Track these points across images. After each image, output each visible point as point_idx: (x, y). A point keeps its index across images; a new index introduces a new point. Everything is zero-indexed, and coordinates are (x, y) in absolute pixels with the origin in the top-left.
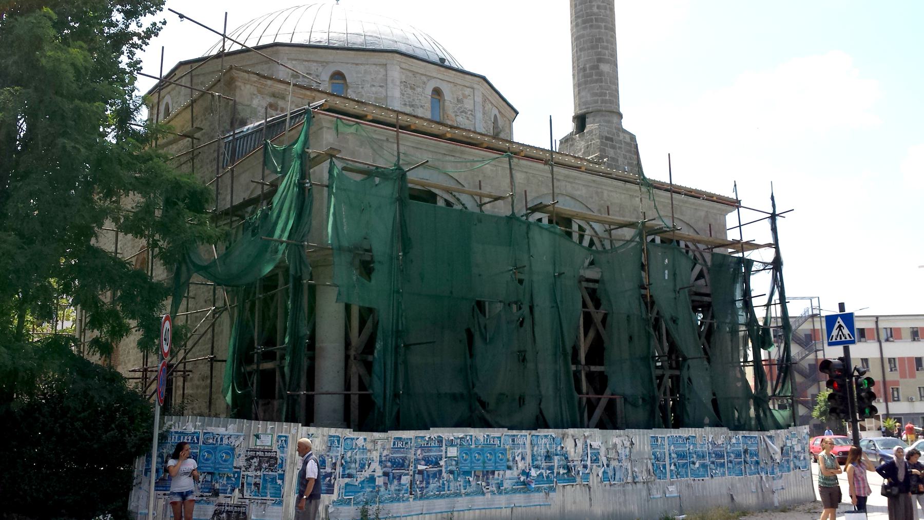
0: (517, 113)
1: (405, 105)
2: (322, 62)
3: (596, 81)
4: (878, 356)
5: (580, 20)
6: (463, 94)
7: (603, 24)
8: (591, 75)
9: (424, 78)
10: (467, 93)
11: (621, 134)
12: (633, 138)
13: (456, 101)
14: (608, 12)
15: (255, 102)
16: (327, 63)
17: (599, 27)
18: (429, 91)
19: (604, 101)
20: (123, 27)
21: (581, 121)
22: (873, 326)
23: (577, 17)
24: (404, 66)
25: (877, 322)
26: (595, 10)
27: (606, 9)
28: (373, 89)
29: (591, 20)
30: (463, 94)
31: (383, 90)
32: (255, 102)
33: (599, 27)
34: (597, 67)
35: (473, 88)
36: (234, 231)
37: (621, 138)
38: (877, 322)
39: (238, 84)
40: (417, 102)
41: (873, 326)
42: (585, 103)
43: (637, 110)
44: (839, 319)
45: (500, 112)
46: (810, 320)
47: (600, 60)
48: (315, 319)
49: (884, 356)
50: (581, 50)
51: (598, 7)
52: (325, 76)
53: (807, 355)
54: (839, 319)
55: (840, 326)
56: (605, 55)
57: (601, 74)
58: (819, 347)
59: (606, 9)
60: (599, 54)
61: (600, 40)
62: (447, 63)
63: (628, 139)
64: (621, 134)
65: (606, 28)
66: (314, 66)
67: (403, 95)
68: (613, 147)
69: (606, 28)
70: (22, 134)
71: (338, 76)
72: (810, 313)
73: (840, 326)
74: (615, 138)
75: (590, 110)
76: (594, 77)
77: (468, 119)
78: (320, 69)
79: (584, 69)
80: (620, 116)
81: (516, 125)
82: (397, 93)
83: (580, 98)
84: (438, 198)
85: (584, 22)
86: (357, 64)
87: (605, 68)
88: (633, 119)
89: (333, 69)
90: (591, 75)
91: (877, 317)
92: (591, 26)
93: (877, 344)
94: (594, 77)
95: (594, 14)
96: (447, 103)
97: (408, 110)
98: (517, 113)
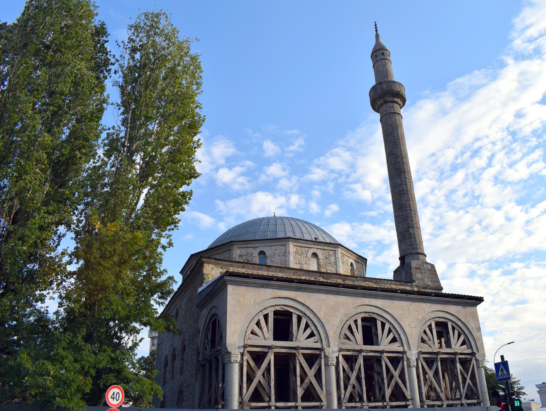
5: (397, 208)
8: (405, 235)
9: (307, 249)
11: (425, 266)
13: (325, 258)
16: (256, 247)
18: (310, 255)
20: (164, 235)
26: (404, 202)
31: (284, 258)
34: (408, 231)
39: (205, 265)
42: (403, 250)
44: (501, 365)
47: (409, 227)
52: (256, 253)
54: (501, 365)
55: (502, 369)
57: (410, 234)
63: (430, 267)
64: (425, 266)
66: (250, 250)
68: (421, 273)
70: (64, 137)
71: (262, 253)
73: (502, 369)
74: (422, 267)
75: (406, 254)
78: (253, 251)
79: (401, 233)
85: (399, 209)
87: (411, 231)
89: (259, 250)
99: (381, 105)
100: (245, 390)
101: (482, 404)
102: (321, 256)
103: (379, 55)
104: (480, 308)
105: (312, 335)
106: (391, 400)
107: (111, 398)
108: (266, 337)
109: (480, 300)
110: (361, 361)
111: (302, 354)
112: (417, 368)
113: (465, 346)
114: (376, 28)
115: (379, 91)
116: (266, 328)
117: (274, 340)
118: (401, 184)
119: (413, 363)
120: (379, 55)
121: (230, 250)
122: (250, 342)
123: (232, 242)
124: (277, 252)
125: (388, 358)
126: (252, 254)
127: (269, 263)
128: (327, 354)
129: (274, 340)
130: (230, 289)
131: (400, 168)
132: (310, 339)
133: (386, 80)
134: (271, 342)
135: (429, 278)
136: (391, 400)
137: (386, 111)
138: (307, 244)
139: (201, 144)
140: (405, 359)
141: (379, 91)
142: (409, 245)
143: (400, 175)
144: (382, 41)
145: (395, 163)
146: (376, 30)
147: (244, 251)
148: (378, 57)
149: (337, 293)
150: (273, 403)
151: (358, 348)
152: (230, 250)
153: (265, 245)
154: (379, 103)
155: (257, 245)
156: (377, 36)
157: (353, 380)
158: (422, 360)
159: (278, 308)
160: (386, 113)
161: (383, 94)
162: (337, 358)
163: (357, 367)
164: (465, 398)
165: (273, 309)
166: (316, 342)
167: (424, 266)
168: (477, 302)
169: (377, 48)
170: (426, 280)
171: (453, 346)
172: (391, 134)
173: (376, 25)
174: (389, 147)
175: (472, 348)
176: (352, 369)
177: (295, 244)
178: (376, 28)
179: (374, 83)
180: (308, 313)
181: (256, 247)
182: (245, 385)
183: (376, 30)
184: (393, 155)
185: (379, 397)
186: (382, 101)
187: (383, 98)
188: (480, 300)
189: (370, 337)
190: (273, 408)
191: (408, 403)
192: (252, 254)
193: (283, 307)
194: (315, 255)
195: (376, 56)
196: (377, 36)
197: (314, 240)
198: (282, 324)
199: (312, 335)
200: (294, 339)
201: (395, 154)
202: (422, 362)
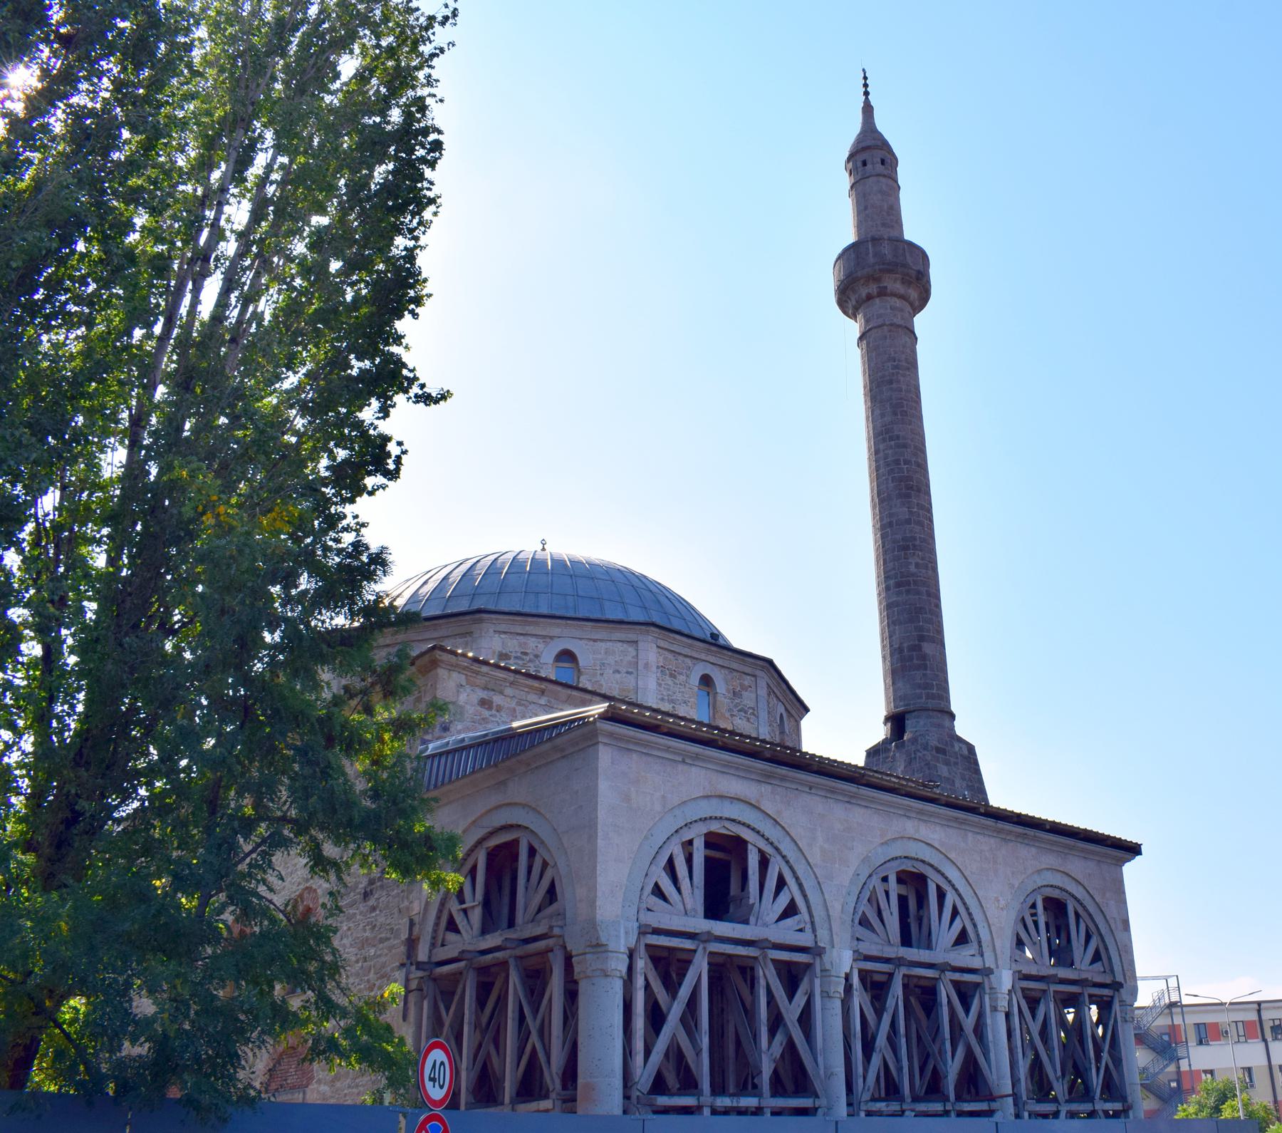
0: (807, 710)
1: (662, 699)
2: (544, 637)
3: (918, 668)
4: (1265, 1063)
5: (892, 582)
6: (741, 685)
7: (924, 589)
8: (911, 658)
9: (688, 661)
10: (746, 683)
11: (957, 746)
12: (971, 749)
13: (731, 695)
14: (930, 572)
15: (463, 698)
16: (551, 638)
17: (918, 593)
18: (695, 680)
19: (933, 697)
21: (897, 722)
22: (1254, 1017)
23: (887, 578)
24: (662, 644)
25: (1259, 1011)
26: (912, 569)
27: (927, 568)
28: (618, 676)
29: (908, 583)
30: (741, 685)
31: (631, 678)
32: (463, 698)
33: (918, 593)
34: (919, 648)
35: (754, 676)
36: (1053, 988)
37: (957, 749)
38: (1259, 1011)
40: (678, 696)
41: (1253, 1016)
42: (901, 698)
43: (978, 709)
45: (786, 709)
46: (1167, 1011)
47: (922, 638)
48: (576, 1032)
49: (1273, 1063)
50: (894, 623)
51: (917, 565)
52: (548, 655)
53: (1165, 1067)
56: (928, 631)
57: (924, 657)
58: (1181, 1052)
59: (927, 568)
60: (921, 629)
61: (920, 610)
62: (721, 642)
63: (965, 752)
65: (929, 595)
66: (532, 642)
67: (660, 685)
68: (947, 763)
69: (929, 595)
71: (567, 656)
72: (1167, 1001)
75: (911, 708)
76: (915, 661)
77: (748, 720)
78: (541, 646)
79: (900, 650)
80: (952, 716)
81: (806, 723)
82: (652, 684)
83: (894, 691)
84: (750, 847)
85: (898, 585)
86: (595, 641)
87: (928, 648)
88: (967, 725)
90: (911, 658)
91: (1259, 1003)
92: (908, 592)
93: (1262, 1045)
94: (915, 661)
95: (913, 575)
96: (719, 698)
97: (666, 707)
98: (807, 710)
99: (869, 297)
100: (639, 1058)
101: (1131, 1113)
102: (721, 687)
103: (872, 162)
104: (1131, 871)
105: (791, 911)
106: (959, 1098)
107: (431, 1079)
108: (685, 911)
109: (1133, 850)
110: (897, 989)
111: (773, 960)
112: (1008, 1015)
113: (1098, 966)
114: (866, 85)
115: (871, 260)
116: (688, 880)
117: (706, 916)
118: (908, 522)
119: (1003, 1004)
120: (872, 162)
121: (471, 633)
122: (654, 920)
123: (479, 611)
124: (611, 660)
125: (956, 984)
126: (537, 656)
127: (585, 682)
128: (828, 966)
129: (706, 916)
130: (605, 756)
131: (909, 478)
132: (789, 921)
133: (894, 234)
134: (701, 924)
135: (963, 779)
136: (959, 1098)
137: (879, 316)
138: (690, 646)
139: (429, 296)
140: (987, 991)
141: (871, 260)
142: (919, 686)
143: (909, 496)
144: (881, 124)
145: (897, 462)
146: (866, 94)
147: (513, 645)
148: (869, 166)
149: (851, 800)
150: (706, 1098)
151: (890, 952)
152: (471, 633)
153: (578, 633)
154: (864, 292)
155: (555, 631)
156: (868, 110)
157: (881, 1041)
158: (1020, 994)
159: (715, 827)
160: (880, 321)
161: (881, 270)
162: (847, 977)
163: (890, 1003)
164: (1101, 1098)
165: (703, 829)
166: (801, 930)
167: (953, 746)
168: (1127, 855)
169: (868, 143)
170: (958, 783)
171: (1077, 964)
172: (891, 382)
173: (865, 78)
174: (882, 415)
175: (1112, 971)
176: (879, 1013)
177: (662, 644)
178: (866, 85)
179: (850, 237)
180: (786, 847)
181: (551, 638)
182: (639, 1045)
183: (866, 94)
184: (891, 439)
185: (921, 1086)
186: (873, 289)
187: (877, 280)
188: (1133, 850)
189: (912, 929)
190: (707, 1111)
191: (994, 1105)
192: (537, 656)
193: (728, 824)
194: (706, 681)
195: (864, 164)
196: (868, 110)
197: (710, 639)
198: (725, 870)
199: (791, 911)
200: (752, 920)
201: (898, 437)
202: (1018, 999)
